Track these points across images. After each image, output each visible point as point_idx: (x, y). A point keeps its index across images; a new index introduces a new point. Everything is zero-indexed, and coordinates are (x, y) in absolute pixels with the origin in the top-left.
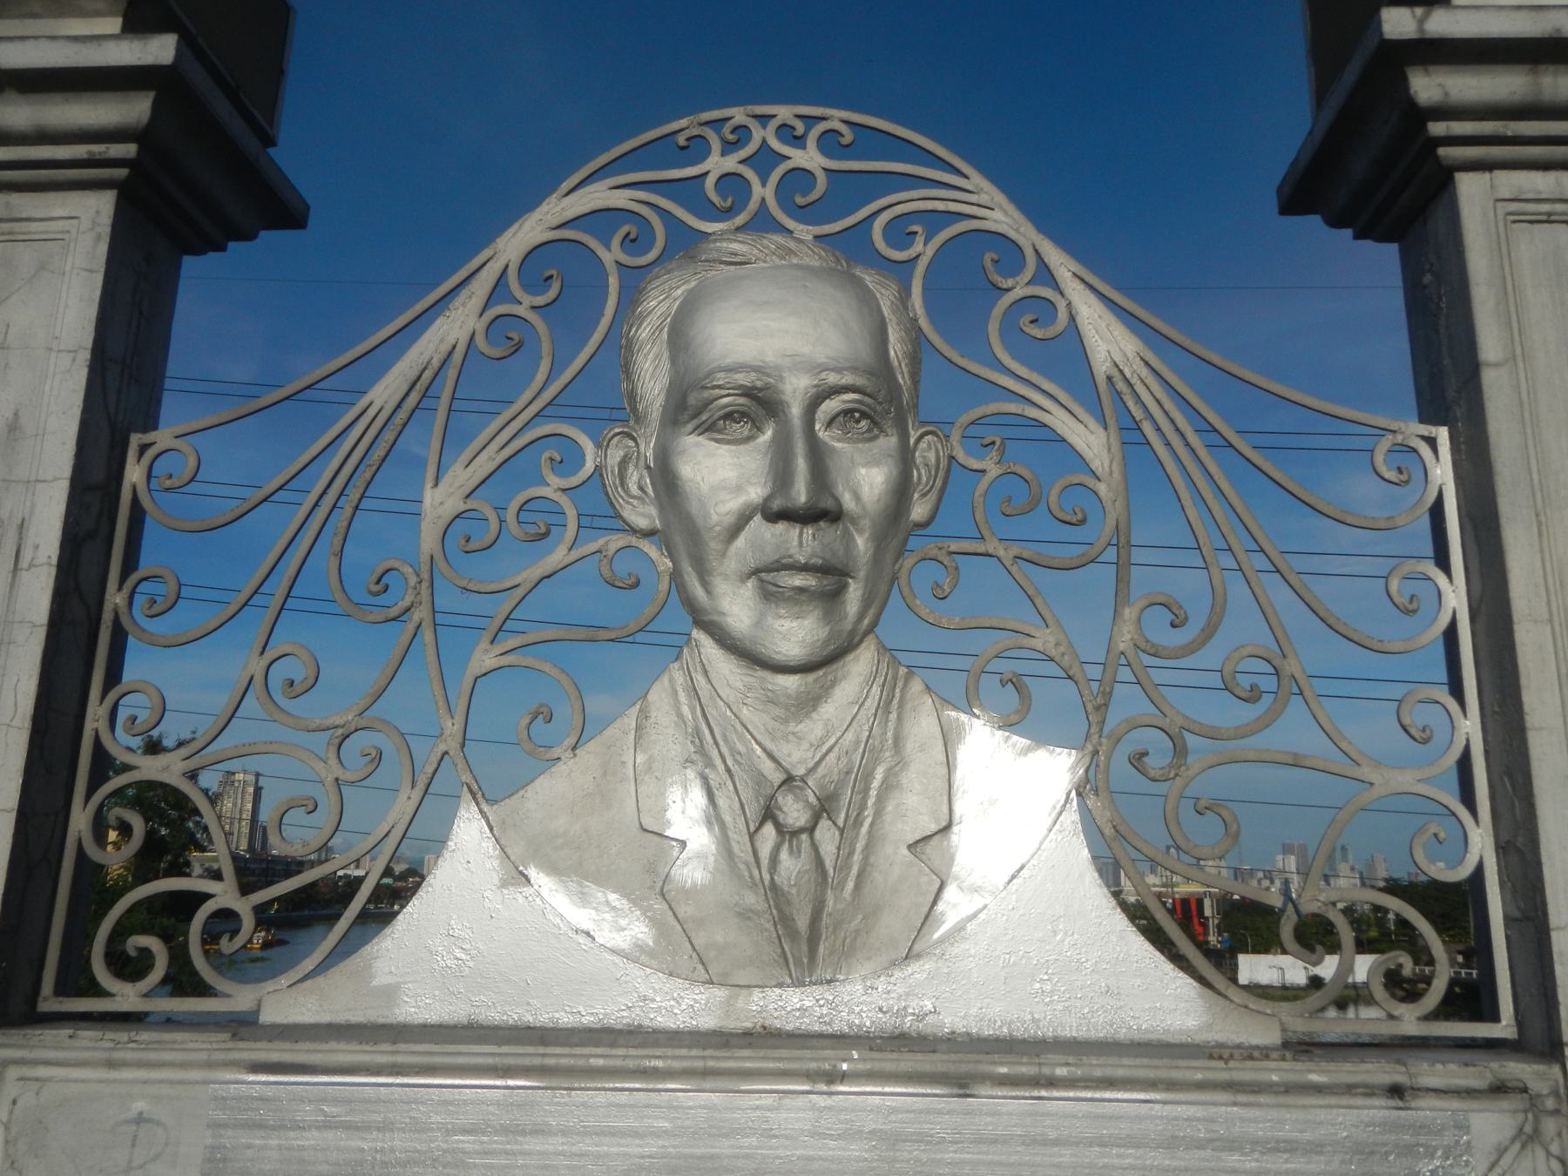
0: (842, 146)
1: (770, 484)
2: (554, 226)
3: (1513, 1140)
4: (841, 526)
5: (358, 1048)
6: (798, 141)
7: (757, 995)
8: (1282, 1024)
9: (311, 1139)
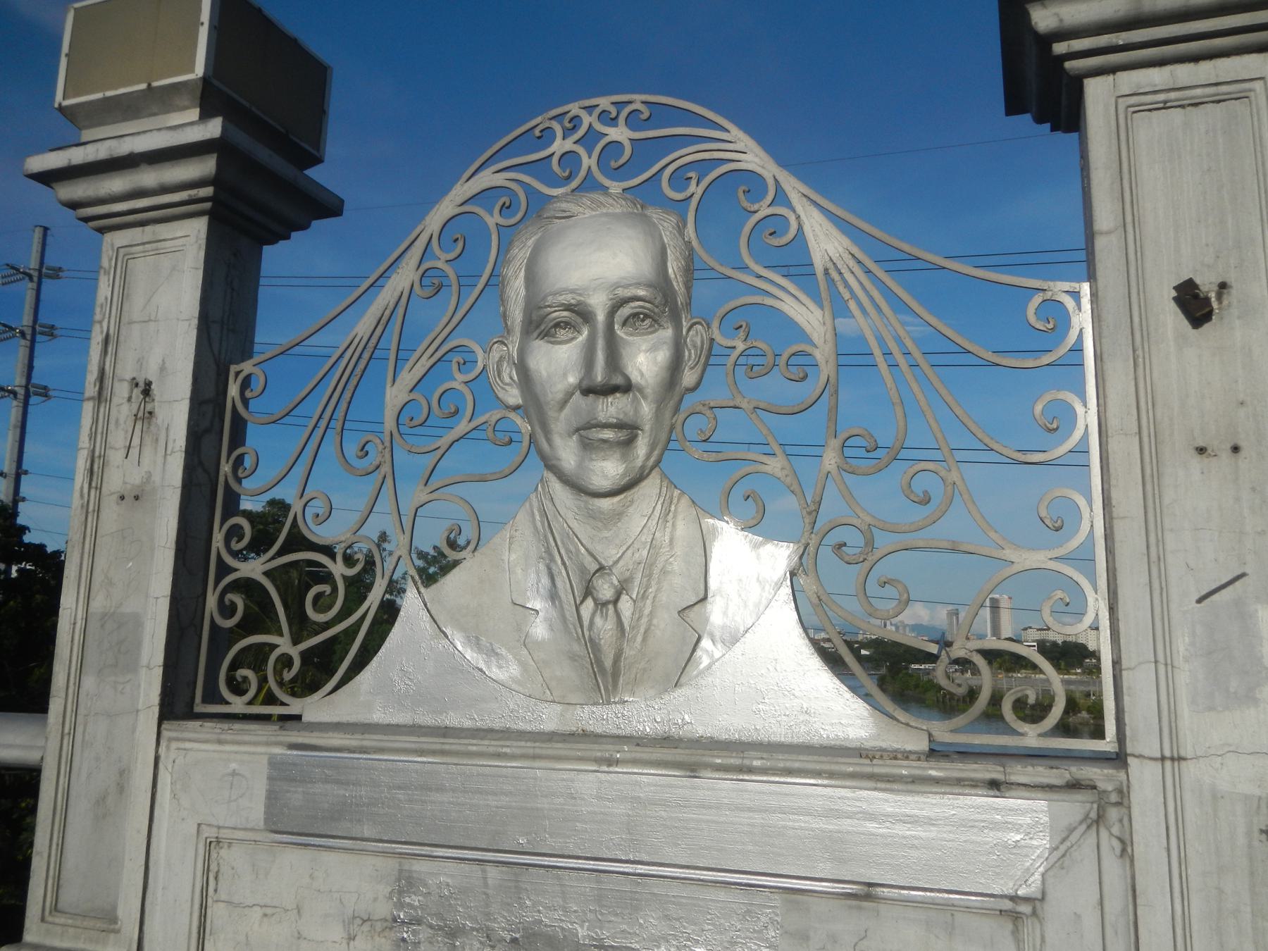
0: (645, 120)
1: (583, 371)
2: (459, 203)
3: (1081, 823)
4: (631, 395)
5: (343, 736)
6: (613, 122)
7: (578, 710)
8: (930, 735)
9: (319, 788)
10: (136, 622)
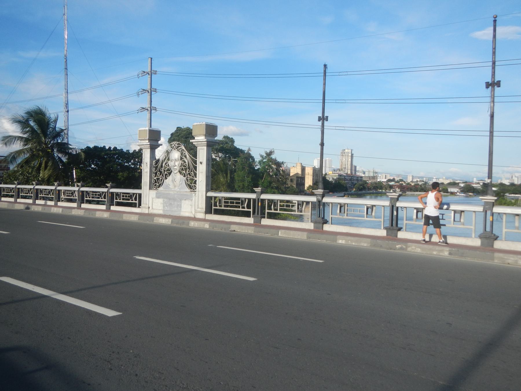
10: (147, 182)
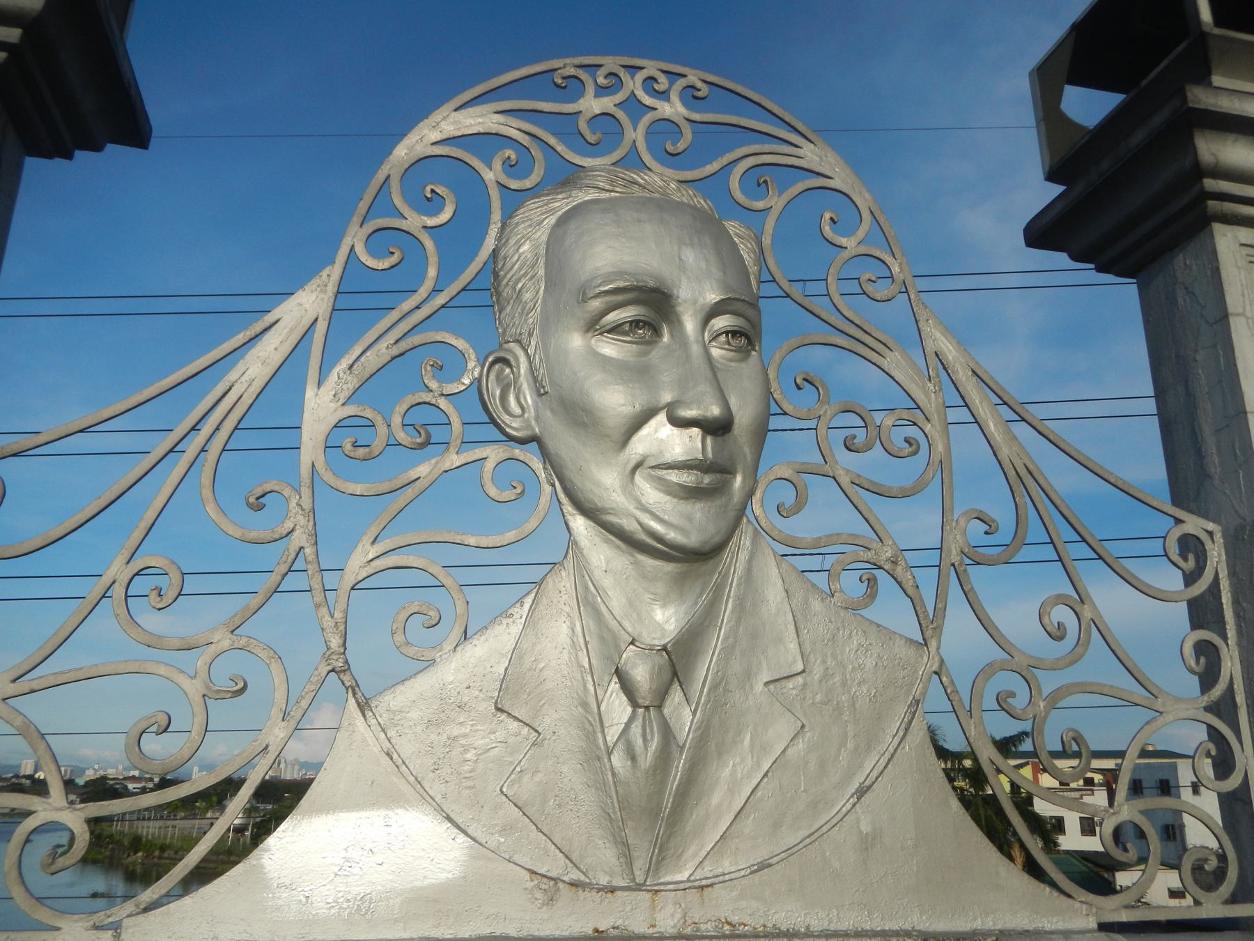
6: (663, 95)
